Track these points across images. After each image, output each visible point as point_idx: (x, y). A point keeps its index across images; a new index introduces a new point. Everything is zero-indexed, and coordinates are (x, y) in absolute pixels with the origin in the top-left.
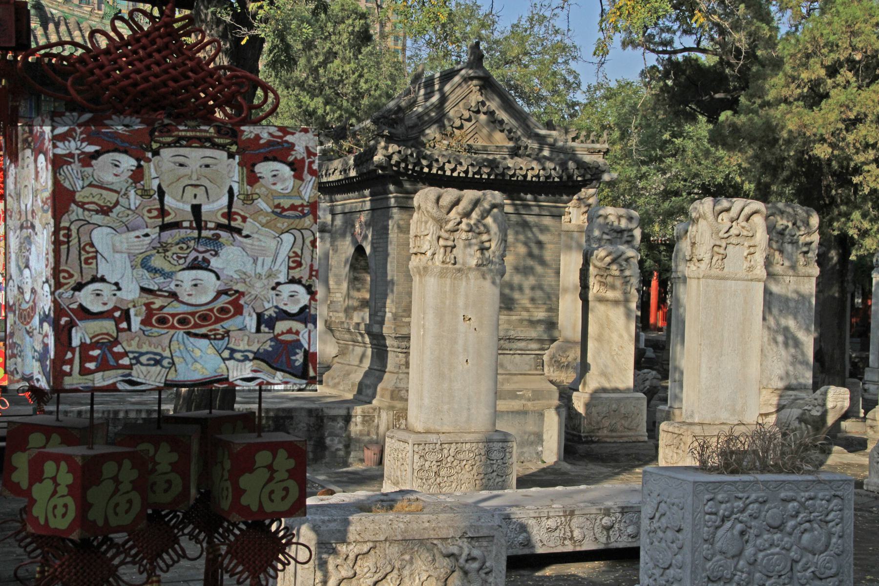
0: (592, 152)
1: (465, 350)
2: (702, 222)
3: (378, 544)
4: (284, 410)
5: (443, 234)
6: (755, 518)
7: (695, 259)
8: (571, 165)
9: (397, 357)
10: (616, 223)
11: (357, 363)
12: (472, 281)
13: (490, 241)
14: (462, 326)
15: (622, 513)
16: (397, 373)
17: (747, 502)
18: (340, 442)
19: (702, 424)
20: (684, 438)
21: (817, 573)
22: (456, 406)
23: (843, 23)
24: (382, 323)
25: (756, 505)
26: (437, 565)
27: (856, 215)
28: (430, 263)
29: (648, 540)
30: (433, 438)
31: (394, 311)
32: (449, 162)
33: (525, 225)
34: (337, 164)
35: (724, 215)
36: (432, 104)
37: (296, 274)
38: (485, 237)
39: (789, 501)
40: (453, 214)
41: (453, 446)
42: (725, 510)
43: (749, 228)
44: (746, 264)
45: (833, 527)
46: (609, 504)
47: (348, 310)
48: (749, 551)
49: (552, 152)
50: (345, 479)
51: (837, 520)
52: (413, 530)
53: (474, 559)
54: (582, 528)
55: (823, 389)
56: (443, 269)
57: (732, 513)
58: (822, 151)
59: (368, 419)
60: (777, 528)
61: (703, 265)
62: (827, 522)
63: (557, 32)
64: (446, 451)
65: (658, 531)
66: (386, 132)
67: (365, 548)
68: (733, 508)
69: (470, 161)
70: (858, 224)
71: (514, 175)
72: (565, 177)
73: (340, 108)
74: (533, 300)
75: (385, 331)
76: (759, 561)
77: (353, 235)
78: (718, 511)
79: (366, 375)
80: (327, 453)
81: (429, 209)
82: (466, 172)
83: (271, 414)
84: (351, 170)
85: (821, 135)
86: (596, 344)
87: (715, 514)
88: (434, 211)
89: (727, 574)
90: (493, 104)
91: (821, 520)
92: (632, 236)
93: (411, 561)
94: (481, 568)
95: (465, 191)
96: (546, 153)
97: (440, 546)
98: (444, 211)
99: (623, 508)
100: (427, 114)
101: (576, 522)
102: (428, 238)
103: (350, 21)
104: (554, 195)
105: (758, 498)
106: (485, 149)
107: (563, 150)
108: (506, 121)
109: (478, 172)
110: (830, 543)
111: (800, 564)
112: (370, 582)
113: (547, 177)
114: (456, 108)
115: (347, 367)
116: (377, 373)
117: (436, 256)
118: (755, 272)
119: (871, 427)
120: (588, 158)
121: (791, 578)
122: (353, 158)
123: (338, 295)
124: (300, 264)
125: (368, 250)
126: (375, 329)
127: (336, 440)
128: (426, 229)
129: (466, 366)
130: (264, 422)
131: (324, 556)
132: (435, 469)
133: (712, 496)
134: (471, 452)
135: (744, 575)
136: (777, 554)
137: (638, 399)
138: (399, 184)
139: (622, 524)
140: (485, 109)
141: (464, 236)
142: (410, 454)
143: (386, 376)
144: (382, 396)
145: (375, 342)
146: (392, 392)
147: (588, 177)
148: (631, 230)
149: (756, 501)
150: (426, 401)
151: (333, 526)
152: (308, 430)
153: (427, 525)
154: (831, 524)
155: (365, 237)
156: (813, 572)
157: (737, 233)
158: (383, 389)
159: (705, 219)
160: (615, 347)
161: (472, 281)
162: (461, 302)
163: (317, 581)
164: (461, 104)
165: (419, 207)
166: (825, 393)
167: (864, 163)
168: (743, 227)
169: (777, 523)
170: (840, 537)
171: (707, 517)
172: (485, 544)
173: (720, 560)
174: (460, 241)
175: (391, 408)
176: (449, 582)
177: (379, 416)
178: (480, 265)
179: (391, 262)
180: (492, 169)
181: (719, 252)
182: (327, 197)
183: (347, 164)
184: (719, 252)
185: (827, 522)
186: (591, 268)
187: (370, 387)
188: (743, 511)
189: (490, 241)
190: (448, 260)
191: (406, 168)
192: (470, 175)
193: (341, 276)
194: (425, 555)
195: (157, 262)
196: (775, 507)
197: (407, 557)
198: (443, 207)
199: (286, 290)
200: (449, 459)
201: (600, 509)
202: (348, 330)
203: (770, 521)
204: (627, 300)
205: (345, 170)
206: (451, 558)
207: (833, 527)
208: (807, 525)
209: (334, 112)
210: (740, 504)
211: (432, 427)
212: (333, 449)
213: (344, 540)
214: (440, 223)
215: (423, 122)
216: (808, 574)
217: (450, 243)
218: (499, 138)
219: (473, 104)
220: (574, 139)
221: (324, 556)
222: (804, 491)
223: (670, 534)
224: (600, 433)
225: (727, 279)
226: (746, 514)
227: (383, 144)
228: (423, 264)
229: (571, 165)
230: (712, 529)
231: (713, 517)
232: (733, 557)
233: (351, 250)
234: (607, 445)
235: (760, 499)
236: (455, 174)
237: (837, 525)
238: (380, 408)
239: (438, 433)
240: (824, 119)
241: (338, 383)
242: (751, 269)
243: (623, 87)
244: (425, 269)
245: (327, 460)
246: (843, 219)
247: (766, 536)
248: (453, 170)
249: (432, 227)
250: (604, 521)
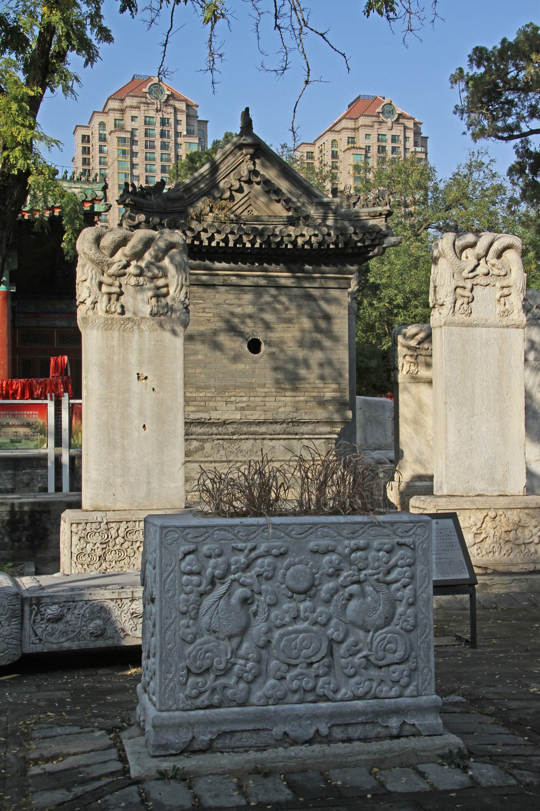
1: (141, 413)
2: (442, 262)
4: (40, 504)
5: (106, 279)
6: (268, 579)
12: (147, 334)
14: (136, 386)
17: (253, 555)
21: (372, 658)
22: (132, 480)
25: (268, 560)
28: (90, 313)
33: (310, 297)
38: (161, 282)
39: (324, 553)
40: (118, 256)
41: (123, 526)
42: (215, 568)
43: (500, 266)
44: (500, 308)
45: (398, 590)
48: (259, 627)
51: (406, 580)
57: (227, 571)
60: (305, 592)
62: (389, 584)
63: (494, 176)
68: (229, 565)
71: (282, 241)
74: (322, 378)
76: (274, 642)
81: (86, 250)
87: (199, 573)
90: (271, 174)
91: (378, 580)
98: (107, 252)
102: (87, 283)
110: (394, 614)
111: (345, 645)
114: (226, 180)
117: (98, 305)
118: (512, 317)
121: (330, 667)
130: (18, 517)
136: (304, 631)
154: (394, 586)
156: (365, 657)
157: (486, 271)
159: (444, 257)
161: (147, 334)
162: (133, 358)
164: (232, 175)
168: (493, 265)
169: (303, 585)
170: (411, 605)
171: (185, 578)
173: (208, 642)
174: (129, 287)
185: (389, 584)
186: (399, 348)
188: (248, 567)
189: (167, 286)
190: (113, 309)
192: (231, 244)
198: (104, 248)
200: (117, 541)
203: (290, 582)
207: (398, 590)
208: (355, 588)
211: (102, 505)
216: (357, 660)
217: (115, 289)
218: (279, 209)
222: (348, 539)
225: (476, 326)
226: (253, 573)
231: (195, 578)
232: (230, 637)
235: (274, 551)
236: (214, 244)
237: (405, 586)
242: (506, 313)
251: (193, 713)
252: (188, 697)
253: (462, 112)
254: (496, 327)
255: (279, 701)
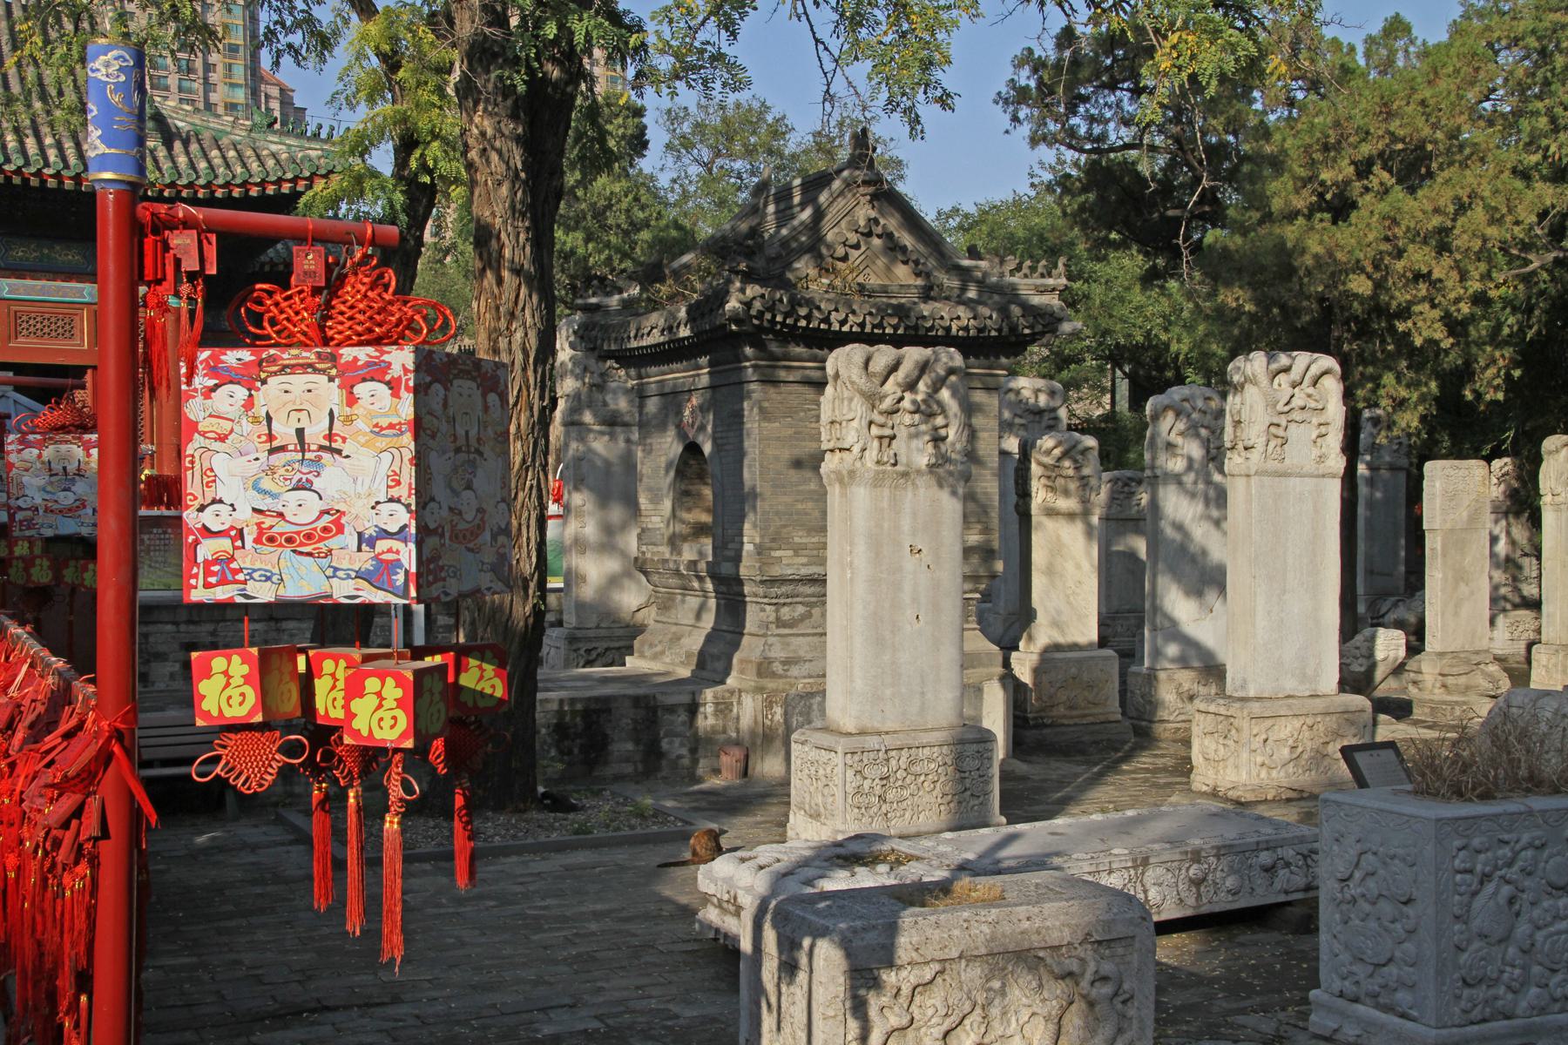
0: (1042, 291)
1: (915, 600)
2: (1250, 390)
3: (947, 965)
4: (597, 699)
6: (1529, 874)
7: (1240, 446)
8: (1016, 310)
9: (763, 610)
10: (1032, 401)
11: (692, 622)
13: (946, 426)
14: (910, 563)
15: (1218, 856)
16: (764, 635)
17: (1518, 847)
18: (682, 745)
19: (1259, 699)
20: (1236, 722)
23: (1377, 100)
24: (737, 559)
25: (1529, 853)
26: (1046, 994)
27: (1388, 379)
28: (858, 464)
29: (1337, 916)
30: (872, 742)
31: (757, 540)
32: (836, 310)
34: (657, 318)
35: (1282, 377)
36: (802, 223)
37: (395, 492)
38: (940, 421)
40: (890, 386)
41: (905, 753)
42: (1485, 865)
44: (1315, 452)
46: (1196, 842)
47: (674, 542)
48: (1523, 929)
49: (980, 292)
50: (704, 804)
52: (1004, 935)
53: (1105, 979)
54: (1160, 885)
55: (1367, 631)
56: (877, 473)
58: (1360, 285)
59: (723, 708)
61: (1255, 456)
64: (893, 762)
65: (1361, 901)
66: (743, 266)
67: (928, 974)
69: (867, 308)
70: (1392, 392)
71: (932, 327)
72: (1006, 330)
73: (608, 245)
75: (743, 572)
76: (1538, 945)
77: (679, 426)
78: (1474, 866)
79: (709, 639)
80: (664, 763)
81: (854, 378)
82: (862, 325)
83: (579, 707)
84: (682, 328)
85: (1358, 261)
86: (1044, 580)
88: (862, 382)
89: (1491, 971)
90: (892, 223)
92: (1056, 419)
93: (1003, 992)
94: (1116, 994)
95: (906, 349)
96: (972, 294)
97: (1049, 961)
98: (877, 381)
99: (1218, 848)
100: (795, 238)
101: (1151, 875)
102: (855, 424)
103: (620, 120)
104: (987, 357)
105: (1534, 839)
106: (884, 290)
107: (998, 289)
108: (910, 247)
109: (880, 325)
112: (938, 1032)
113: (980, 330)
114: (836, 230)
115: (674, 629)
116: (729, 636)
117: (867, 453)
119: (1415, 683)
120: (1037, 300)
122: (684, 309)
123: (656, 519)
124: (398, 483)
125: (707, 448)
126: (726, 569)
127: (677, 741)
128: (850, 409)
129: (917, 626)
130: (568, 719)
131: (862, 992)
132: (878, 790)
133: (1465, 841)
134: (934, 762)
135: (1517, 971)
137: (1106, 658)
138: (759, 345)
139: (1219, 874)
140: (879, 230)
141: (907, 419)
142: (839, 769)
143: (745, 640)
144: (742, 672)
145: (723, 589)
146: (760, 665)
147: (1039, 328)
148: (1054, 410)
149: (1530, 845)
150: (859, 684)
151: (872, 937)
152: (635, 729)
153: (1026, 924)
155: (702, 428)
158: (741, 661)
160: (1070, 583)
162: (906, 523)
163: (849, 1038)
164: (843, 223)
165: (837, 376)
166: (1373, 639)
167: (1410, 303)
168: (1309, 396)
171: (1459, 877)
172: (1120, 951)
175: (759, 690)
176: (1065, 1021)
177: (739, 703)
178: (933, 465)
179: (750, 466)
180: (900, 319)
181: (1276, 433)
182: (633, 372)
183: (675, 318)
184: (1276, 433)
186: (1034, 466)
187: (718, 658)
188: (1510, 864)
189: (946, 426)
191: (773, 321)
193: (659, 489)
194: (1027, 979)
195: (266, 483)
196: (1558, 854)
197: (996, 984)
198: (874, 374)
199: (386, 508)
201: (1186, 853)
202: (677, 573)
203: (1554, 878)
204: (1086, 514)
205: (670, 328)
206: (1068, 980)
209: (600, 252)
210: (1506, 852)
211: (869, 724)
212: (673, 756)
213: (890, 964)
214: (872, 399)
215: (787, 252)
217: (887, 432)
218: (903, 273)
219: (862, 223)
220: (1012, 273)
221: (862, 992)
223: (1386, 908)
224: (1055, 713)
226: (1516, 868)
227: (738, 284)
228: (847, 465)
229: (1016, 310)
230: (1466, 898)
231: (1468, 877)
232: (1500, 942)
233: (678, 449)
234: (1063, 729)
235: (1537, 843)
236: (846, 329)
238: (740, 691)
239: (879, 734)
240: (1356, 237)
241: (663, 653)
242: (1321, 458)
243: (987, 213)
244: (852, 473)
245: (664, 773)
246: (1370, 385)
247: (1546, 904)
248: (843, 323)
249: (859, 407)
250: (1191, 872)
251: (1469, 1029)
252: (1465, 1011)
253: (1006, 102)
254: (1312, 476)
255: (1543, 1011)
